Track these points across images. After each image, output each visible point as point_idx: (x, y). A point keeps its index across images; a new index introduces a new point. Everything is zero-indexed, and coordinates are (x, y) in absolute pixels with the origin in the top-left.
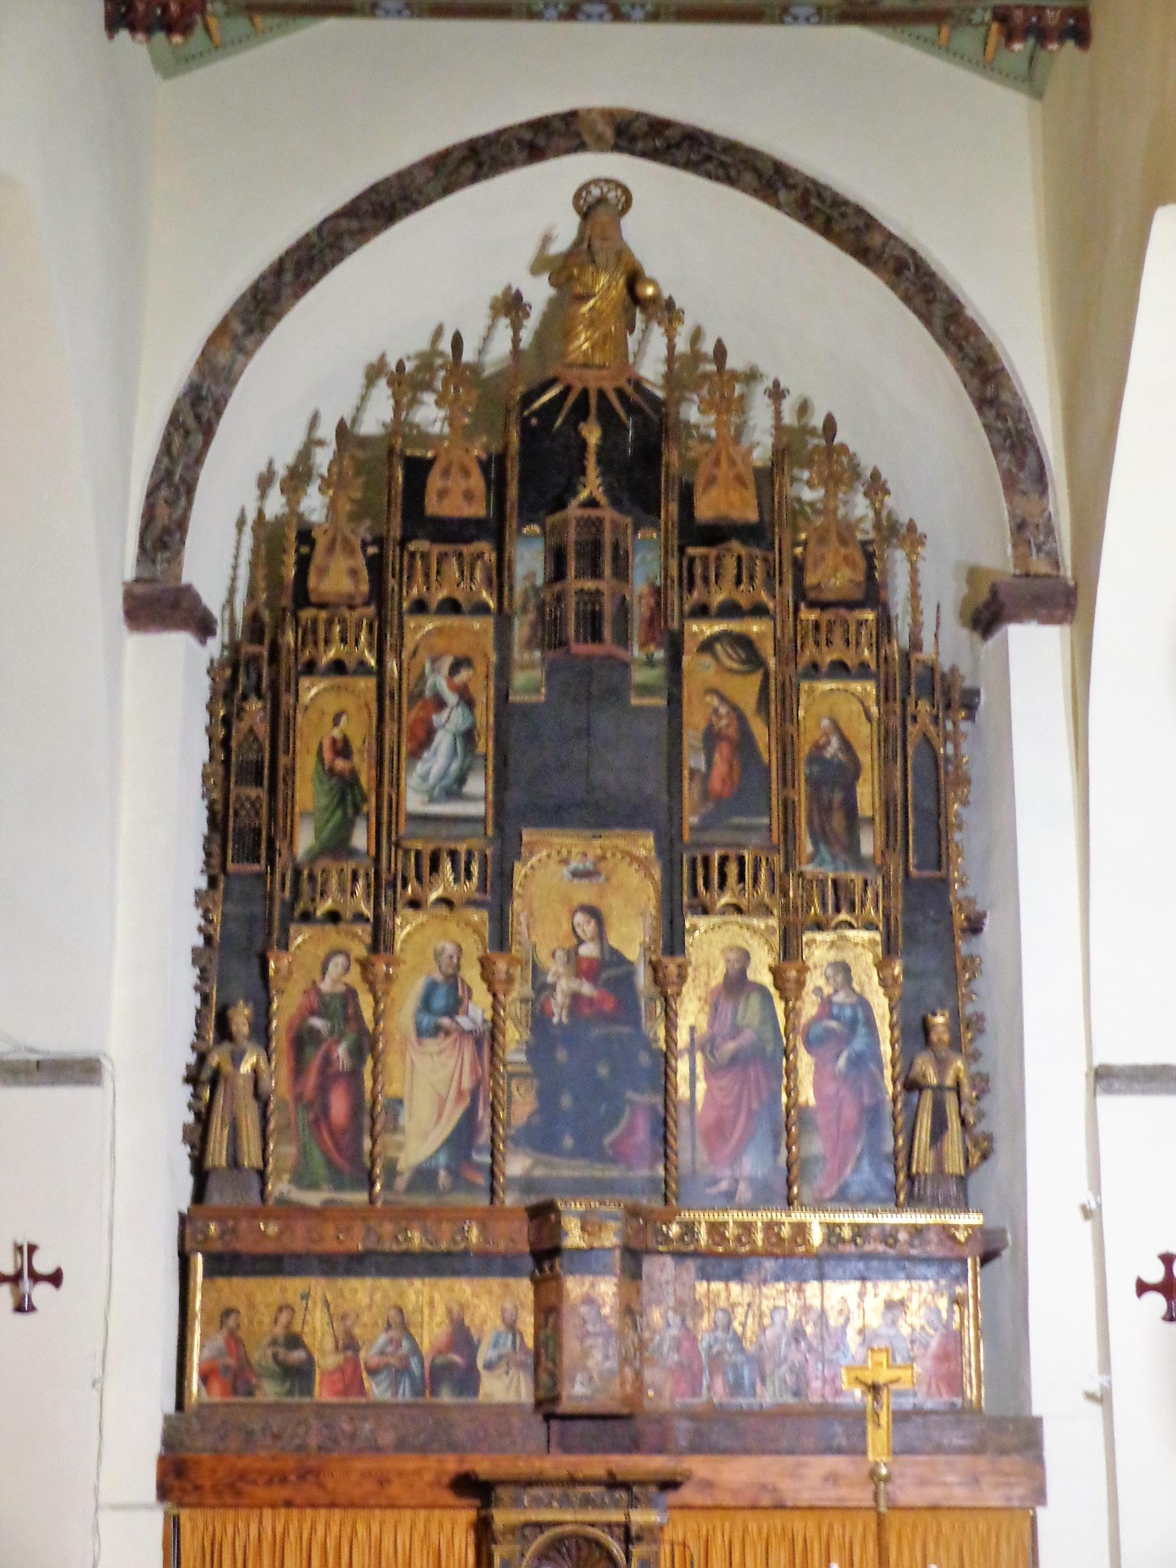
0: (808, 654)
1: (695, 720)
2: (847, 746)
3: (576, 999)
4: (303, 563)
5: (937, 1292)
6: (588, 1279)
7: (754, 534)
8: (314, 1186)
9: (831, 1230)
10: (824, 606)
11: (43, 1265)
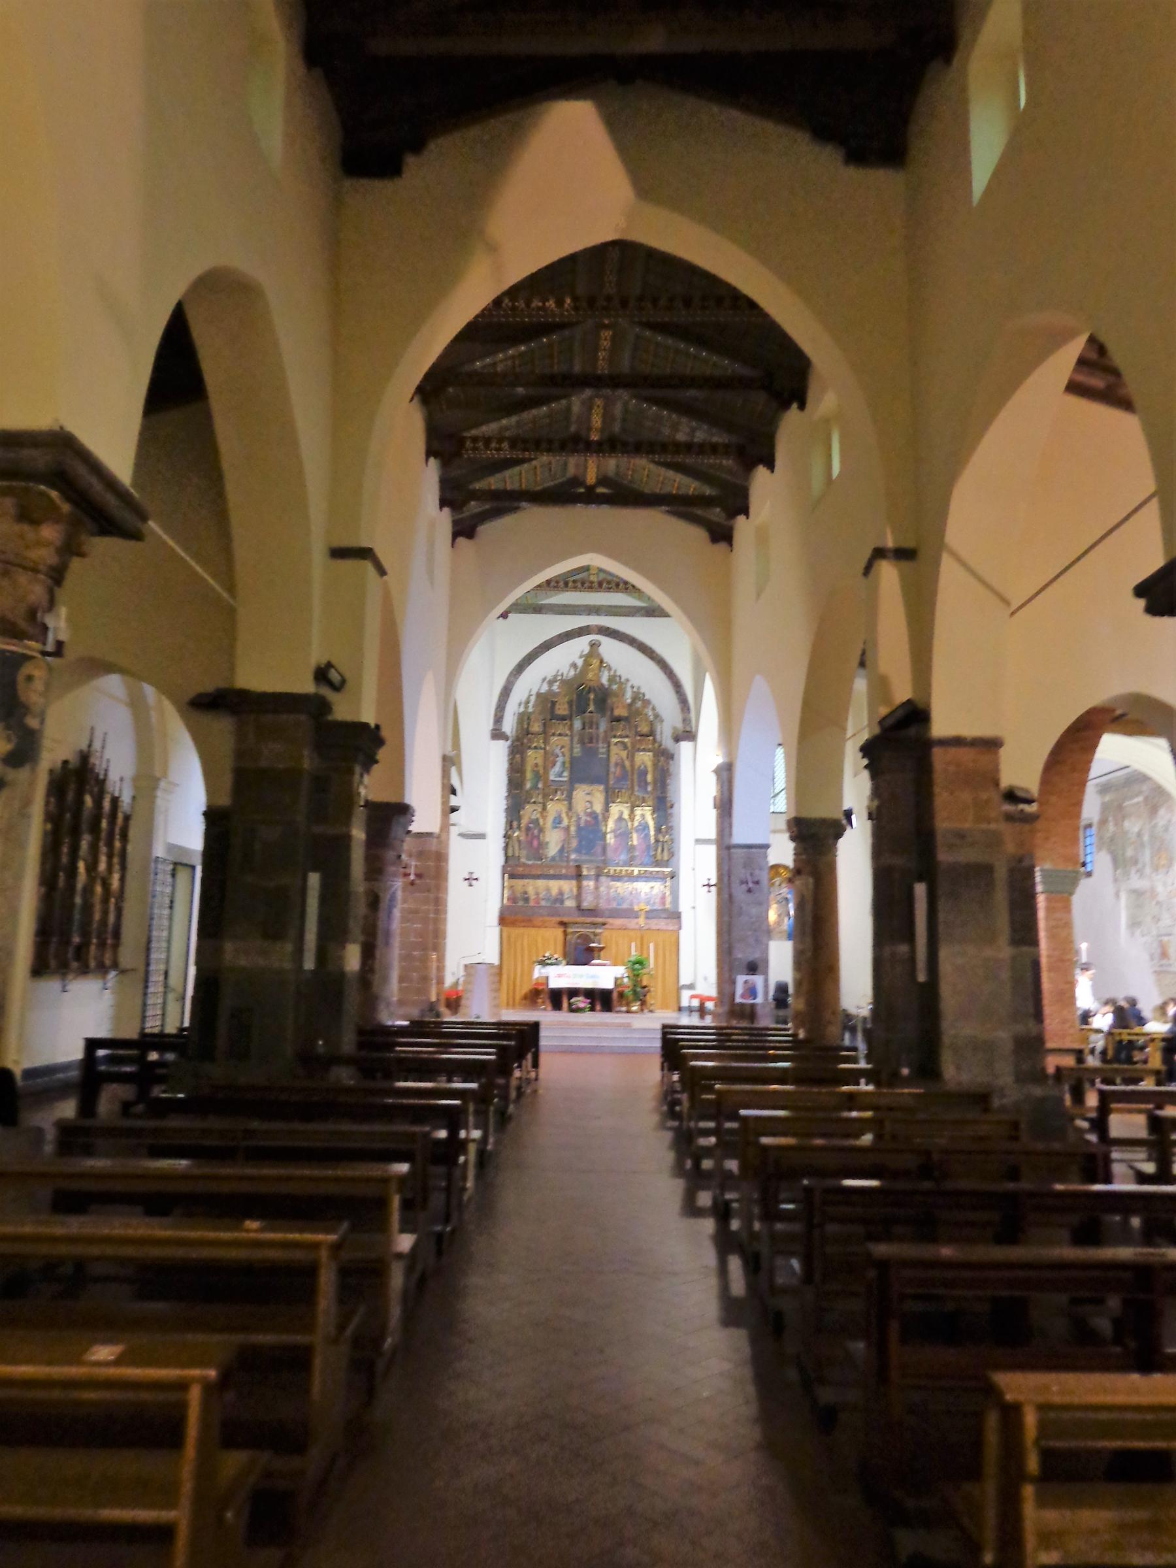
0: (638, 746)
1: (613, 759)
2: (645, 767)
4: (528, 724)
5: (661, 885)
6: (588, 881)
7: (626, 719)
8: (530, 860)
9: (639, 871)
10: (642, 735)
11: (706, 888)
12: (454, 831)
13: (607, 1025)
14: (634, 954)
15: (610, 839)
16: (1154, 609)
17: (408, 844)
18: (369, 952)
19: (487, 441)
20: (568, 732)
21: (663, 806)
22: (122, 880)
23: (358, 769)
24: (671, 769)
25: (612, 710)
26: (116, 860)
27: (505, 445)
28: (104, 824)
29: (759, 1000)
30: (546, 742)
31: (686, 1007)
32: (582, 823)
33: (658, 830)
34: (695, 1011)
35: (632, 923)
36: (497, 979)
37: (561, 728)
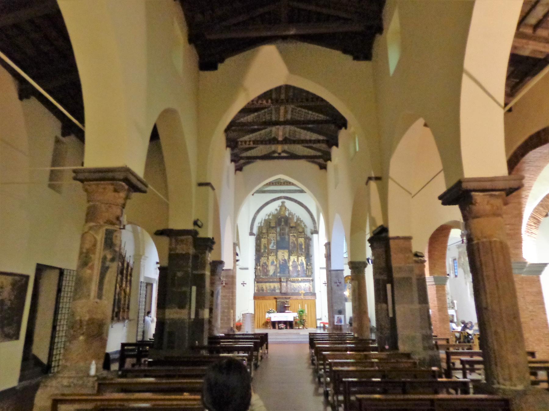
1: (291, 241)
2: (302, 243)
3: (282, 262)
7: (295, 227)
9: (301, 279)
11: (324, 284)
12: (238, 267)
13: (290, 334)
14: (300, 308)
15: (291, 268)
16: (444, 204)
17: (223, 273)
18: (211, 310)
19: (245, 142)
20: (276, 233)
21: (308, 256)
22: (130, 289)
23: (207, 252)
24: (311, 244)
25: (290, 224)
26: (128, 283)
27: (251, 143)
28: (125, 272)
29: (343, 323)
30: (268, 236)
31: (319, 327)
32: (281, 263)
33: (307, 265)
34: (322, 328)
35: (299, 297)
36: (253, 319)
37: (273, 231)
